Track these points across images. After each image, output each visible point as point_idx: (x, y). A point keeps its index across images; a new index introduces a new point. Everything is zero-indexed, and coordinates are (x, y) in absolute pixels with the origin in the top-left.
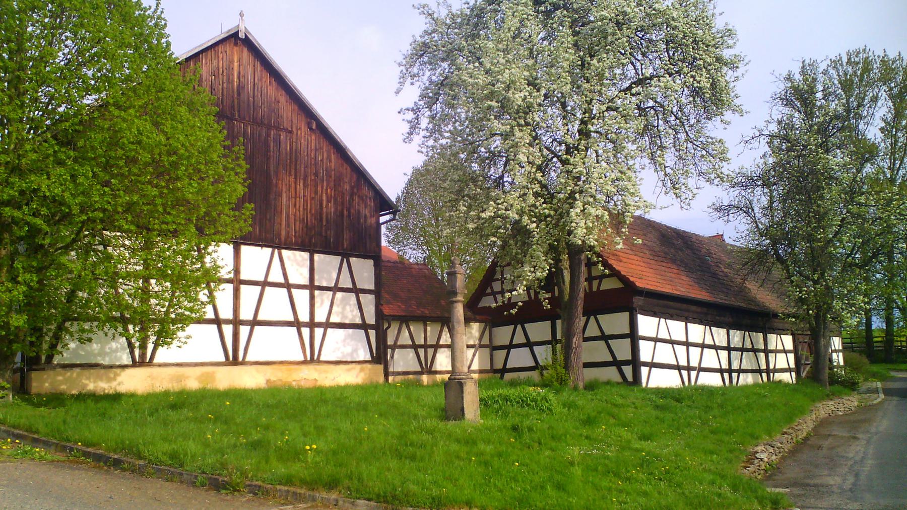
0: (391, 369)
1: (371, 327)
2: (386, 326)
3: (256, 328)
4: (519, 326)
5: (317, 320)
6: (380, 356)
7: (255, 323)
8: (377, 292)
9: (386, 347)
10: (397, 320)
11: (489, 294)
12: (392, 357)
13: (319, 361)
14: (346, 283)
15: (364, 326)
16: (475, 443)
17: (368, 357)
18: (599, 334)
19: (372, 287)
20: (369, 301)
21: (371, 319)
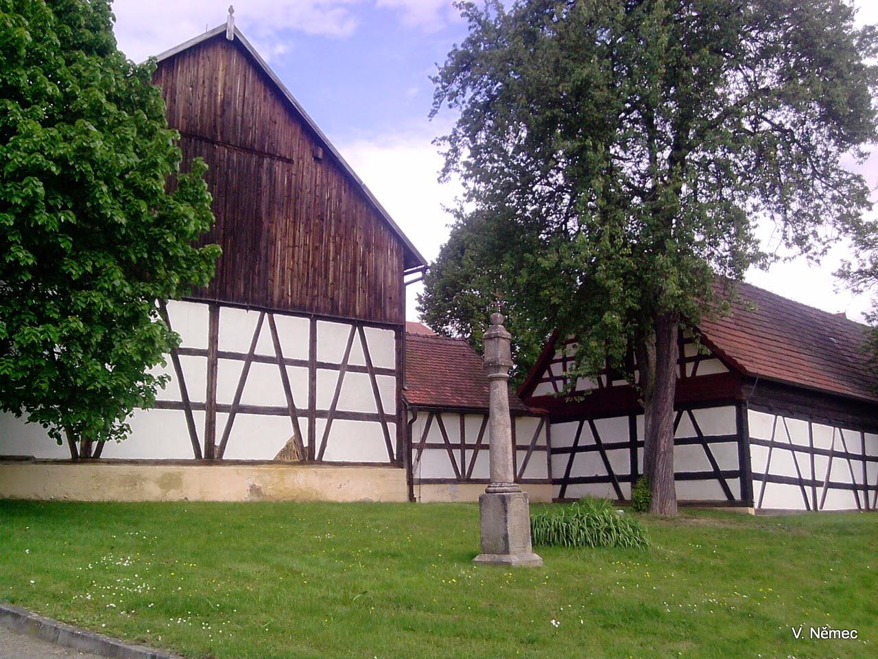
0: (416, 476)
1: (391, 418)
2: (410, 418)
4: (586, 423)
6: (403, 457)
9: (411, 446)
11: (547, 380)
14: (358, 359)
15: (381, 417)
20: (388, 385)
21: (390, 408)
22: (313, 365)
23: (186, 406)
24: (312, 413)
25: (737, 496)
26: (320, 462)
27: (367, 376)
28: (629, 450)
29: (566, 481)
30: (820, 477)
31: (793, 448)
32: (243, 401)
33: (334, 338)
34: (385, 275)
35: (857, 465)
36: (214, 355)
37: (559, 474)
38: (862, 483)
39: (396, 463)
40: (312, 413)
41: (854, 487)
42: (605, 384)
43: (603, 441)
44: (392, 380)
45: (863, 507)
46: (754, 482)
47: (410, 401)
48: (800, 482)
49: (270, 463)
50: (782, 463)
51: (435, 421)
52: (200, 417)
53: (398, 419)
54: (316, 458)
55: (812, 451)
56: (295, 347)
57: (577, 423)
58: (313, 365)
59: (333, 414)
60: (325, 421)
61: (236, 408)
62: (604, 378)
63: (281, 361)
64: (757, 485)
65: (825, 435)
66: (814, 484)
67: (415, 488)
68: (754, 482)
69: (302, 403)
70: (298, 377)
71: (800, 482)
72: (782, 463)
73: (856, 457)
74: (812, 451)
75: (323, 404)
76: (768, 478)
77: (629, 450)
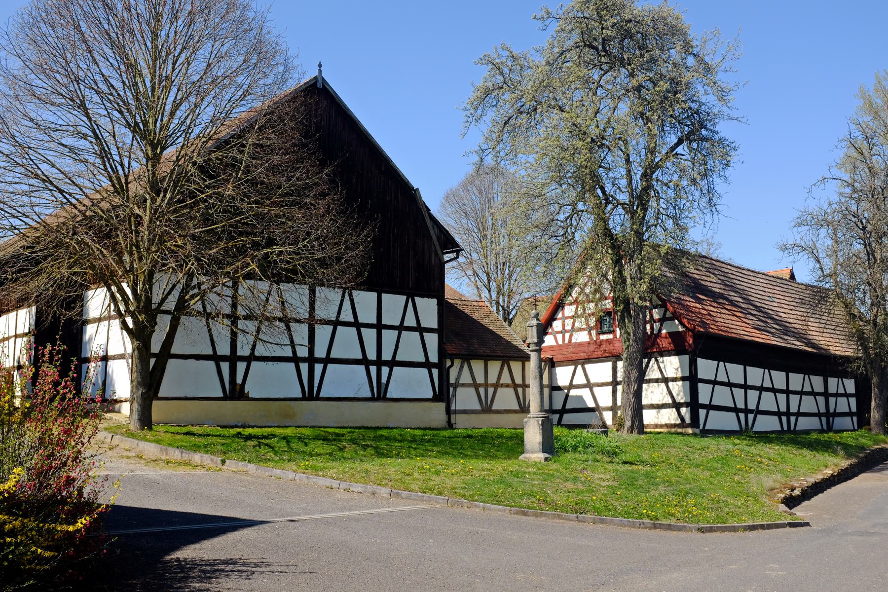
0: (453, 408)
1: (434, 365)
2: (448, 363)
4: (579, 367)
8: (439, 330)
9: (449, 385)
11: (551, 334)
12: (454, 396)
14: (410, 321)
17: (430, 395)
19: (435, 326)
20: (432, 340)
21: (434, 358)
22: (379, 326)
24: (233, 359)
25: (688, 420)
26: (318, 398)
29: (563, 411)
30: (752, 406)
31: (730, 385)
32: (333, 355)
33: (394, 305)
35: (782, 397)
36: (312, 322)
37: (558, 406)
38: (829, 379)
39: (436, 398)
40: (311, 360)
41: (779, 414)
43: (592, 381)
45: (785, 428)
46: (701, 410)
48: (735, 410)
50: (722, 396)
52: (304, 367)
53: (440, 365)
55: (746, 387)
56: (367, 315)
57: (573, 367)
58: (379, 326)
59: (393, 363)
60: (322, 365)
61: (328, 360)
62: (594, 332)
63: (356, 324)
64: (702, 413)
65: (796, 380)
66: (747, 411)
67: (452, 417)
68: (701, 410)
69: (372, 355)
70: (370, 335)
71: (735, 410)
72: (722, 396)
73: (781, 391)
74: (746, 387)
75: (387, 356)
76: (710, 407)
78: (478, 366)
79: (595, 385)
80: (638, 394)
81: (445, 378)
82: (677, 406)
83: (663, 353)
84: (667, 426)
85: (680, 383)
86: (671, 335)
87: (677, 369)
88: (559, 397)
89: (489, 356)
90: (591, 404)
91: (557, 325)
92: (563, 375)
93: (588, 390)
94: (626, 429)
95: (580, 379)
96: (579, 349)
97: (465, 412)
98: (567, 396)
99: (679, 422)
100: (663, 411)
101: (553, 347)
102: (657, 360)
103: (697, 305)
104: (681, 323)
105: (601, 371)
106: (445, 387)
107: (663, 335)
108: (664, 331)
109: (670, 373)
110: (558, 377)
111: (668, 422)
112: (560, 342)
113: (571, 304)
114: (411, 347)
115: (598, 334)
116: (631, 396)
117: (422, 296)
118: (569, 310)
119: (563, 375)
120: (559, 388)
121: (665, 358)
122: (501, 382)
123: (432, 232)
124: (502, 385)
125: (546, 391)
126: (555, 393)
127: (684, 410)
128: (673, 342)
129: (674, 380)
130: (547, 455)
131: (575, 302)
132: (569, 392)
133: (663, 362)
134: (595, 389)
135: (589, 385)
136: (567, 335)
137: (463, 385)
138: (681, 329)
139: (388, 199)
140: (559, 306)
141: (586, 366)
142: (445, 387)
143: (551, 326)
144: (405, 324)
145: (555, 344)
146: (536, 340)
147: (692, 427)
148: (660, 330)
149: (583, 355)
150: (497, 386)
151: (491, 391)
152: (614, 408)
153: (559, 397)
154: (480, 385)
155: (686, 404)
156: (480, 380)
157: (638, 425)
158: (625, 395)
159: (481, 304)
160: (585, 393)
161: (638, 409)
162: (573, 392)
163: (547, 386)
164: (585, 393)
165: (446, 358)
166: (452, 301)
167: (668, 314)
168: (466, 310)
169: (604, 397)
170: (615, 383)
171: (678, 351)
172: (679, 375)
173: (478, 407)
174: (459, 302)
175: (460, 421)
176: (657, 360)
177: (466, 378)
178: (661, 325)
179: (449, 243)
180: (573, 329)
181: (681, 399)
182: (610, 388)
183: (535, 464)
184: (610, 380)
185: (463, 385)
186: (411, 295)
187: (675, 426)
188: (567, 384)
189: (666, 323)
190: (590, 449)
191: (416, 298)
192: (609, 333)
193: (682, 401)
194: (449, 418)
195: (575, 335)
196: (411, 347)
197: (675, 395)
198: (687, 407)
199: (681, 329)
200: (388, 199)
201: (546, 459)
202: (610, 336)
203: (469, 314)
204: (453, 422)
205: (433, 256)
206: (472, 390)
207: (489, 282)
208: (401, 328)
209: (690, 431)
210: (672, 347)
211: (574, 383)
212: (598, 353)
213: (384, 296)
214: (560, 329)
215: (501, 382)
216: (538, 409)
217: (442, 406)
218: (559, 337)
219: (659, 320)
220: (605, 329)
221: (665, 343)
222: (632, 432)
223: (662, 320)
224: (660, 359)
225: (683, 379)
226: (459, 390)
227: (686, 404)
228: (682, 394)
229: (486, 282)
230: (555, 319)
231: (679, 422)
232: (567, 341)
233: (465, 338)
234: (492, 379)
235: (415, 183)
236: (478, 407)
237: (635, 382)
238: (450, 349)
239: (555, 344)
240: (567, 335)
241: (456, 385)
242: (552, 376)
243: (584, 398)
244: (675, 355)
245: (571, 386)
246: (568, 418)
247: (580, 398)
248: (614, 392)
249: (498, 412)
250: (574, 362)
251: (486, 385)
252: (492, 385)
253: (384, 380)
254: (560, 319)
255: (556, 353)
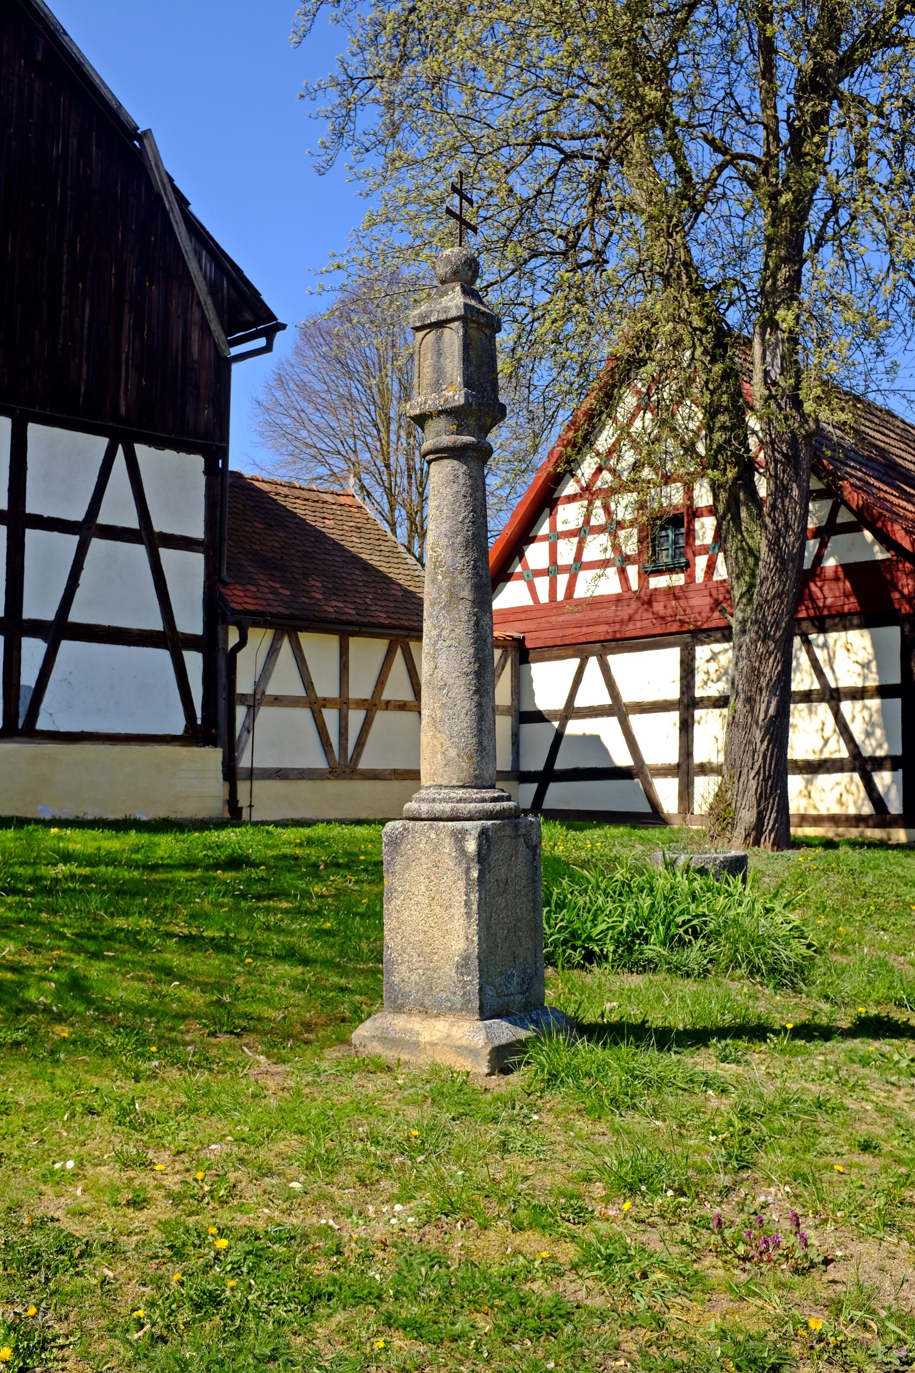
0: (244, 763)
1: (192, 642)
2: (233, 637)
3: (66, 646)
4: (593, 662)
5: (30, 612)
6: (214, 723)
7: (59, 630)
8: (211, 547)
9: (233, 699)
10: (265, 625)
11: (520, 577)
12: (249, 729)
13: (30, 733)
14: (118, 510)
15: (169, 639)
16: (337, 1039)
17: (177, 725)
18: (156, 624)
19: (197, 531)
20: (187, 572)
21: (190, 621)
23: (315, 705)
27: (140, 551)
28: (26, 615)
29: (547, 776)
34: (186, 338)
37: (535, 762)
39: (195, 735)
42: (634, 586)
43: (627, 697)
44: (197, 560)
47: (234, 605)
49: (322, 821)
51: (286, 646)
53: (208, 643)
54: (20, 726)
57: (575, 662)
62: (632, 571)
67: (243, 787)
77: (26, 615)
78: (320, 649)
79: (640, 707)
80: (778, 730)
81: (223, 680)
82: (863, 765)
83: (827, 621)
84: (834, 820)
85: (874, 703)
86: (850, 570)
87: (865, 666)
88: (537, 739)
89: (351, 623)
90: (622, 758)
91: (536, 555)
92: (549, 682)
93: (614, 721)
94: (740, 831)
95: (593, 692)
96: (595, 614)
97: (280, 774)
98: (559, 736)
99: (867, 809)
100: (823, 780)
101: (524, 610)
102: (807, 643)
103: (904, 504)
104: (884, 538)
105: (649, 673)
106: (222, 704)
107: (829, 573)
108: (830, 563)
109: (846, 675)
110: (535, 686)
111: (836, 810)
112: (544, 598)
113: (572, 499)
114: (117, 585)
115: (645, 574)
116: (758, 734)
117: (159, 443)
118: (569, 515)
119: (549, 682)
120: (538, 717)
121: (832, 636)
122: (386, 696)
123: (193, 265)
124: (388, 705)
125: (503, 725)
126: (528, 729)
127: (884, 779)
128: (857, 591)
129: (858, 694)
130: (505, 1032)
131: (588, 492)
132: (563, 726)
133: (825, 645)
134: (635, 720)
135: (618, 709)
136: (563, 580)
137: (277, 701)
138: (880, 554)
139: (57, 150)
140: (545, 500)
141: (613, 660)
142: (222, 704)
143: (522, 556)
144: (103, 519)
145: (530, 602)
146: (456, 396)
147: (906, 826)
148: (819, 558)
149: (602, 631)
150: (371, 706)
151: (356, 718)
152: (686, 770)
153: (537, 739)
154: (326, 702)
155: (892, 762)
156: (327, 687)
157: (775, 823)
158: (739, 734)
159: (343, 500)
160: (607, 730)
161: (777, 769)
162: (575, 727)
163: (507, 711)
164: (607, 730)
165: (226, 623)
166: (265, 487)
167: (844, 516)
168: (300, 509)
169: (658, 739)
170: (688, 705)
171: (871, 613)
172: (873, 682)
173: (320, 763)
174: (285, 491)
175: (264, 799)
176: (807, 643)
177: (285, 680)
178: (823, 545)
179: (249, 315)
180: (580, 559)
181: (876, 745)
182: (674, 717)
183: (446, 1090)
184: (673, 693)
185: (277, 701)
186: (123, 435)
187: (858, 820)
188: (559, 704)
189: (835, 541)
190: (693, 955)
191: (141, 450)
192: (671, 570)
193: (880, 753)
194: (233, 792)
195: (584, 576)
196: (117, 585)
197: (858, 736)
198: (894, 769)
199: (880, 554)
200: (57, 150)
201: (503, 1060)
202: (679, 579)
203: (309, 519)
204: (243, 801)
205: (195, 335)
206: (304, 715)
207: (392, 510)
208: (87, 529)
209: (900, 835)
210: (852, 604)
211: (579, 703)
212: (644, 624)
213: (34, 430)
214: (545, 564)
215: (386, 696)
216: (464, 769)
217: (212, 757)
218: (541, 584)
219: (819, 533)
220: (665, 558)
221: (830, 594)
222: (757, 843)
223: (825, 533)
224: (817, 638)
225: (883, 692)
226: (265, 713)
227: (892, 762)
228: (878, 732)
229: (386, 507)
230: (533, 540)
231: (867, 809)
232: (560, 596)
233: (277, 570)
234: (361, 689)
235: (139, 114)
236: (320, 763)
237: (772, 693)
238: (239, 598)
239: (530, 602)
240: (563, 580)
241: (254, 703)
242: (521, 685)
243: (604, 740)
244: (860, 627)
245: (570, 712)
246: (559, 795)
247: (595, 741)
248: (686, 727)
249: (374, 775)
250: (580, 649)
251: (343, 704)
252: (361, 704)
253: (28, 677)
254: (545, 538)
255: (530, 625)
